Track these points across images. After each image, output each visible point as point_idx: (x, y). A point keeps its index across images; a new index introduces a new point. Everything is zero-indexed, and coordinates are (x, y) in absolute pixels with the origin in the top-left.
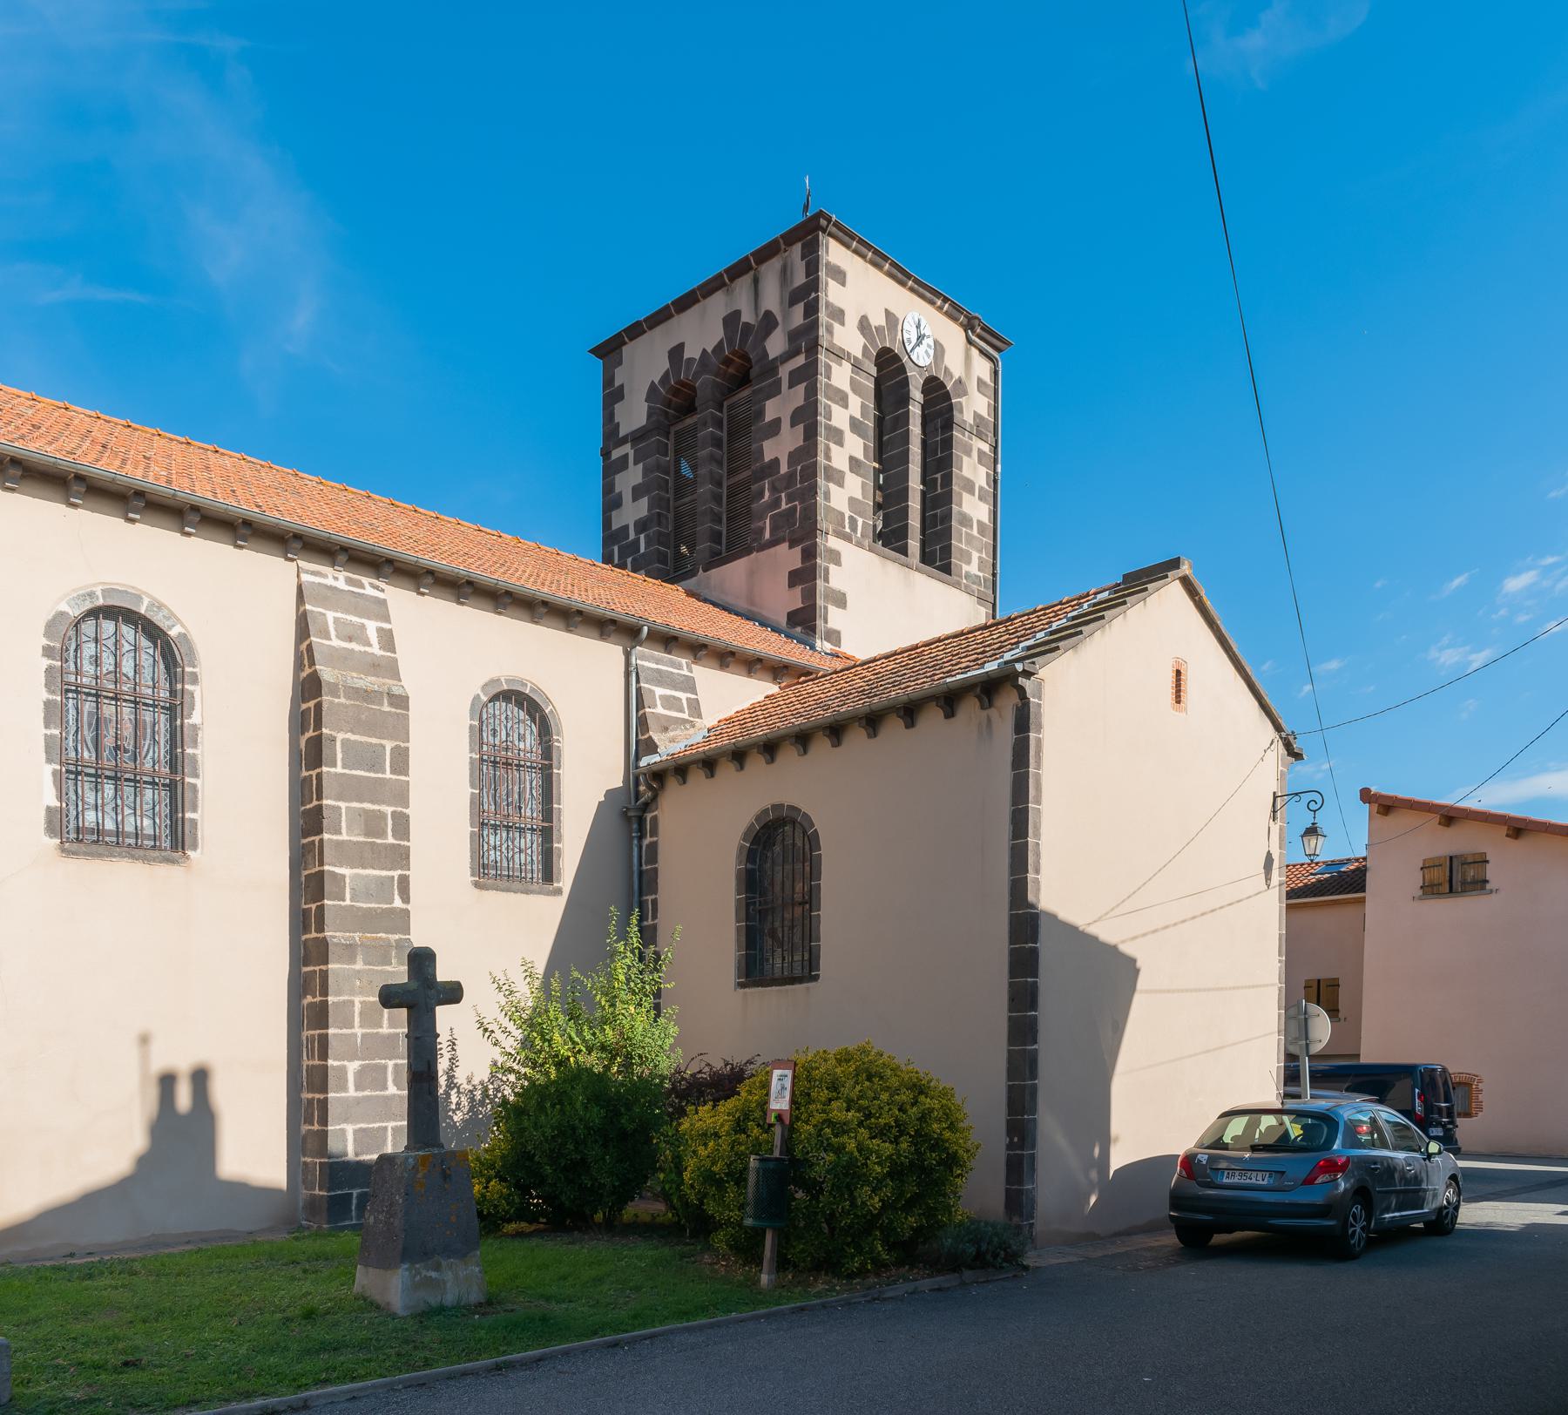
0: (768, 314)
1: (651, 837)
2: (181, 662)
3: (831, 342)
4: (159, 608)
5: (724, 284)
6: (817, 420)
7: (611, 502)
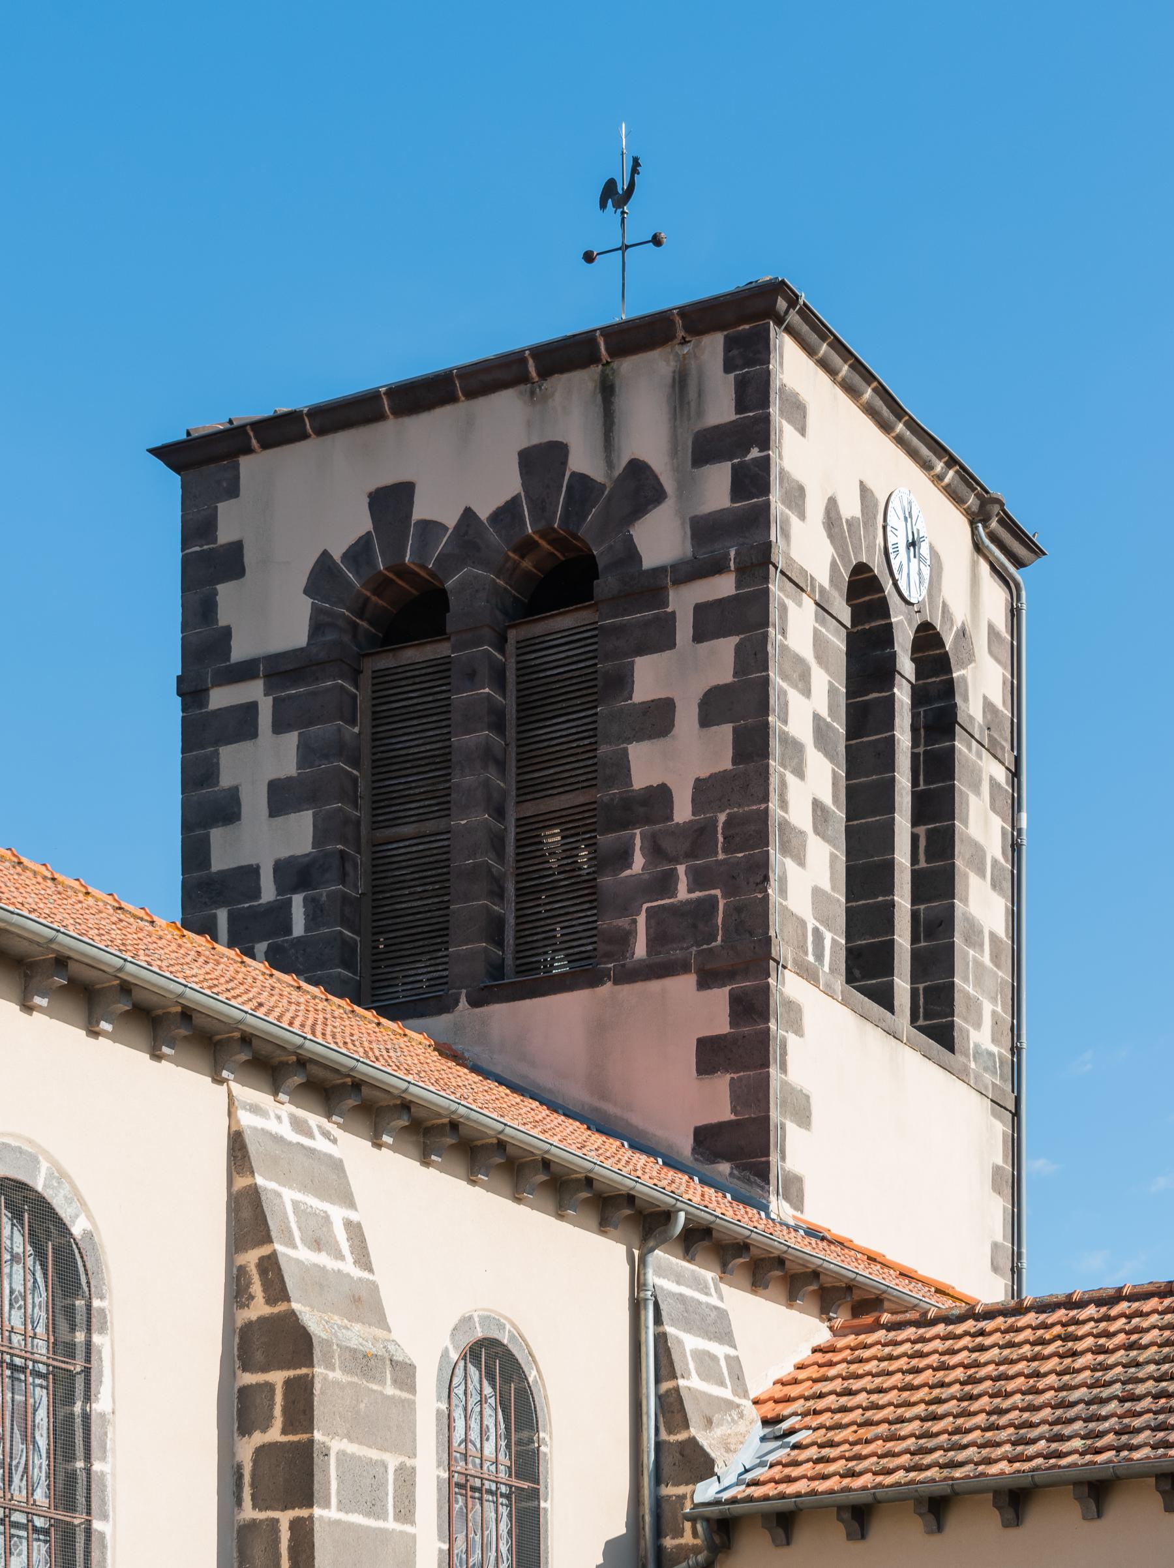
0: (638, 468)
2: (86, 1289)
5: (524, 379)
6: (767, 723)
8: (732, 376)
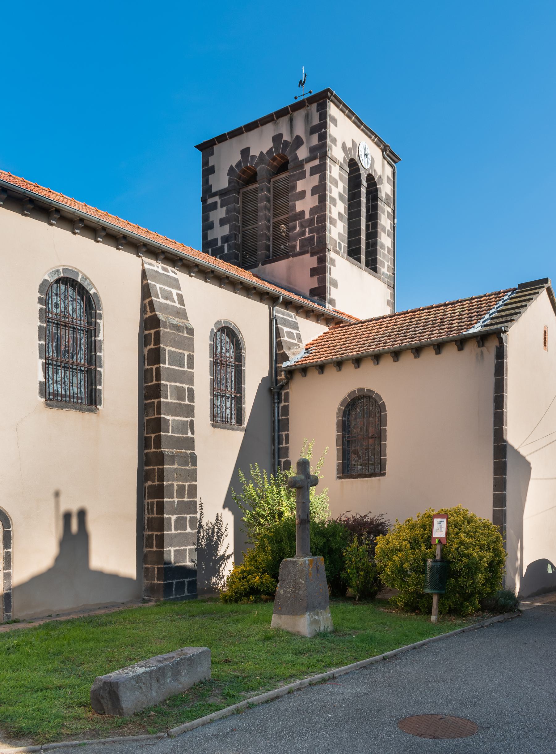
0: (298, 137)
1: (284, 402)
3: (331, 155)
4: (85, 279)
7: (207, 226)
8: (318, 113)
